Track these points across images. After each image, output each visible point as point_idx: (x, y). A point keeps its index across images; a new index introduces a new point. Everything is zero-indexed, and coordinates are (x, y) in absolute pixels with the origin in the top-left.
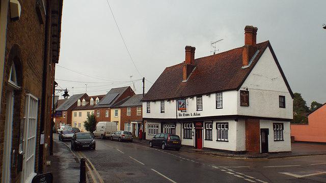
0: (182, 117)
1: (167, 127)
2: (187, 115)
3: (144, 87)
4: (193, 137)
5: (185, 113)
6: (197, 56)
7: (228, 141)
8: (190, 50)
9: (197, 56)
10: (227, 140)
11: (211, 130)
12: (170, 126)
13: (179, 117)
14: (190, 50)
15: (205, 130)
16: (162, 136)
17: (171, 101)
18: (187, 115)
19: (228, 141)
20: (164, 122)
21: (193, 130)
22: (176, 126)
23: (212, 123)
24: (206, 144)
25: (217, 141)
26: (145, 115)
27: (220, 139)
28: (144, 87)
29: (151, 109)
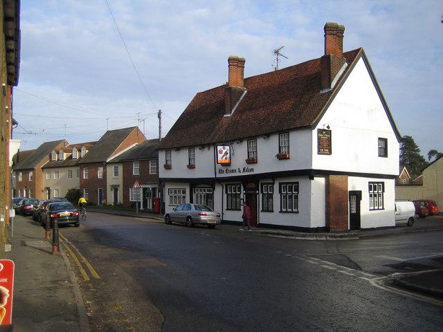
2: (233, 171)
3: (160, 127)
7: (298, 212)
8: (236, 64)
10: (296, 210)
13: (219, 176)
17: (206, 149)
19: (298, 212)
23: (273, 184)
24: (264, 218)
28: (160, 127)
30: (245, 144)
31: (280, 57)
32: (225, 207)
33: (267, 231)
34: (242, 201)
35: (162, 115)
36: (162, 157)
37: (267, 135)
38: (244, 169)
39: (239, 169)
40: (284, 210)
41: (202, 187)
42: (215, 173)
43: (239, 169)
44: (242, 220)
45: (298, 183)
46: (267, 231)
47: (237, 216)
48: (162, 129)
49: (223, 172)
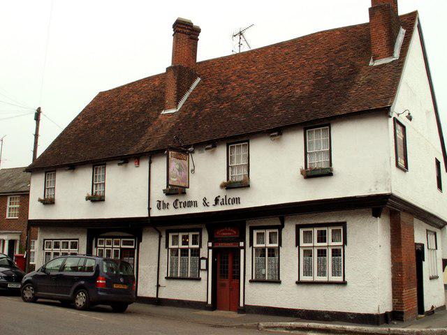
0: (171, 212)
1: (108, 246)
2: (189, 204)
3: (36, 136)
4: (203, 275)
5: (182, 199)
6: (207, 50)
7: (344, 283)
8: (186, 33)
9: (207, 50)
10: (340, 279)
11: (273, 252)
12: (117, 243)
13: (156, 213)
14: (186, 33)
15: (249, 250)
16: (91, 263)
17: (132, 165)
18: (189, 204)
19: (344, 283)
20: (96, 229)
21: (16, 206)
22: (140, 240)
23: (280, 228)
24: (255, 295)
25: (299, 283)
26: (36, 212)
27: (309, 279)
28: (36, 136)
29: (59, 196)
30: (222, 152)
31: (238, 37)
32: (163, 274)
33: (305, 324)
34: (203, 263)
35: (42, 116)
36: (37, 188)
37: (276, 131)
38: (217, 200)
39: (205, 200)
40: (303, 278)
41: (105, 237)
42: (149, 209)
43: (205, 200)
44: (427, 308)
45: (344, 224)
46: (305, 324)
47: (199, 291)
48: (33, 149)
49: (166, 206)
